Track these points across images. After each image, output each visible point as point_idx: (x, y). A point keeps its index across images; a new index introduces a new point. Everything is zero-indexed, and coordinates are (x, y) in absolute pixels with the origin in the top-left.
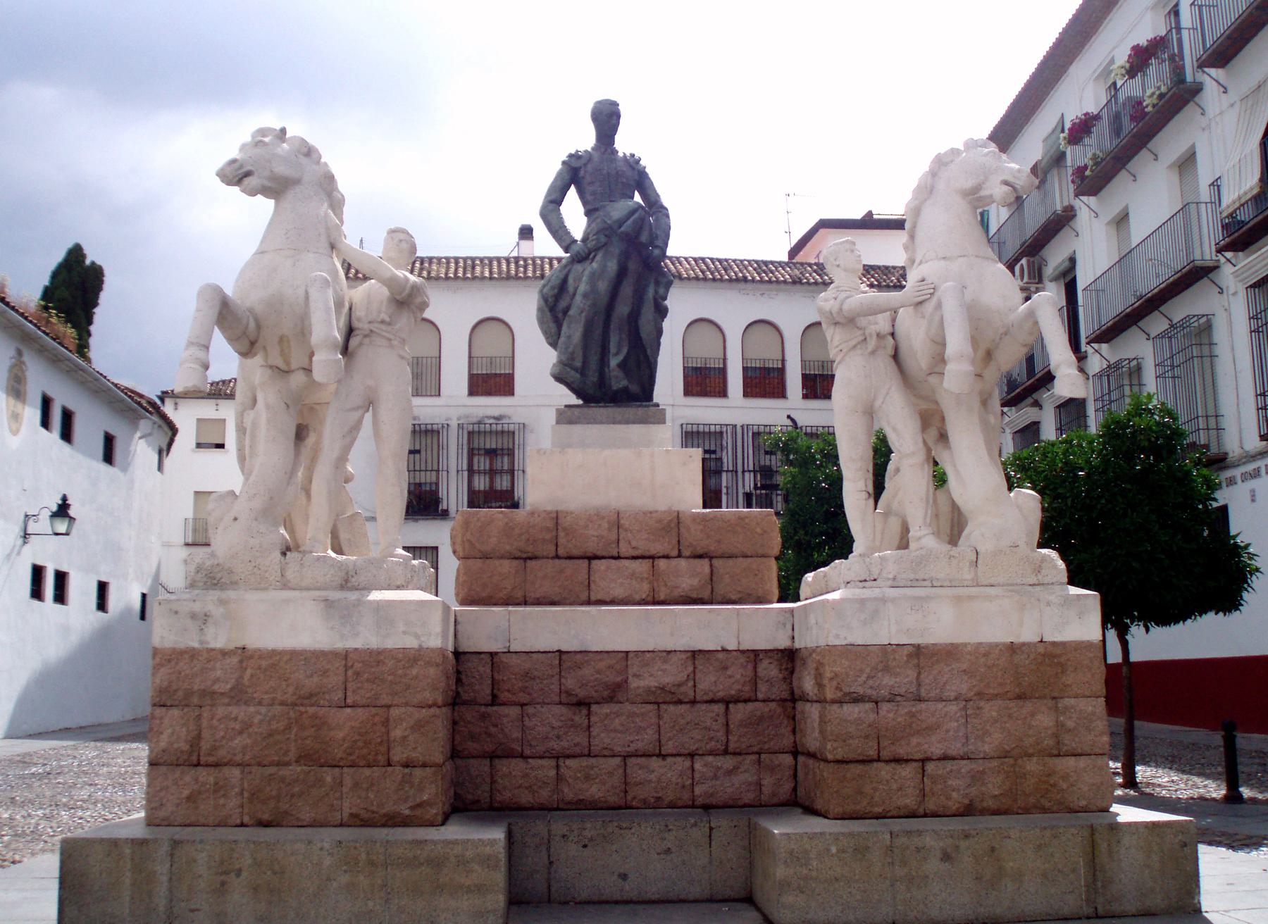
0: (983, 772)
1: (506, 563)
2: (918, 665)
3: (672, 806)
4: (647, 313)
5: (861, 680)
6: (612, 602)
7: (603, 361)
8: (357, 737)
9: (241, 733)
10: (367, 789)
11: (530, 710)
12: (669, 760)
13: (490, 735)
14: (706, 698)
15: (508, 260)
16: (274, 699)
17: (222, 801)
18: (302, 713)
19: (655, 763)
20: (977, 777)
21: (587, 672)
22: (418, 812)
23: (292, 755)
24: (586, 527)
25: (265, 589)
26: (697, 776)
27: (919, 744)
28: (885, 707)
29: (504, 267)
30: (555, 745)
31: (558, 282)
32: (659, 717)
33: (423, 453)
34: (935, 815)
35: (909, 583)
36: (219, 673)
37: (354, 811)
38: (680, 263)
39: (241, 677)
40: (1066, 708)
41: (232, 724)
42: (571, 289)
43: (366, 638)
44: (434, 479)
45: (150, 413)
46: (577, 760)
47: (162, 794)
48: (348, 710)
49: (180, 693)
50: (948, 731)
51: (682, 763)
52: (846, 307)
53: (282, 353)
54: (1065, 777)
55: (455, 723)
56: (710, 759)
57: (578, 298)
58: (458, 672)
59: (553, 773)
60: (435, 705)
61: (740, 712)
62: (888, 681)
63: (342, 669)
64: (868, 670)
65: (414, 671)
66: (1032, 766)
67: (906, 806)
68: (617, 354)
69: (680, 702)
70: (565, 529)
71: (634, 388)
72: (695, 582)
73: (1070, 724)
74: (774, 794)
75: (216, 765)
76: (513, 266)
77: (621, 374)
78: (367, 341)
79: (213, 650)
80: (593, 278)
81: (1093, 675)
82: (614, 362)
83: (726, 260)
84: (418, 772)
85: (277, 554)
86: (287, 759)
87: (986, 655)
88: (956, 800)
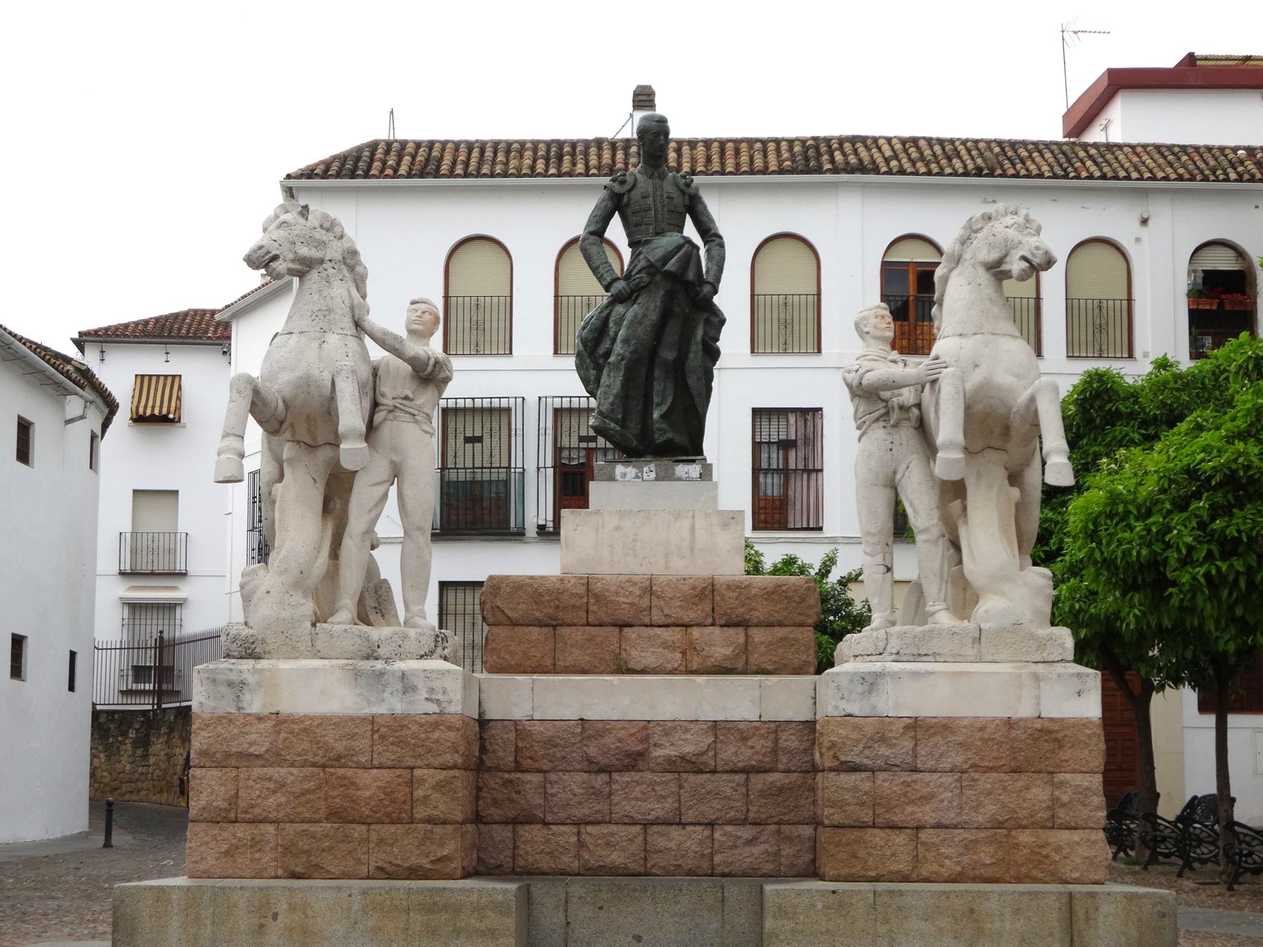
0: (976, 841)
1: (536, 630)
2: (915, 737)
3: (690, 873)
4: (695, 356)
5: (857, 750)
6: (643, 672)
7: (647, 412)
8: (383, 796)
9: (275, 792)
10: (391, 845)
11: (553, 777)
12: (689, 828)
13: (512, 801)
14: (726, 768)
15: (613, 145)
16: (306, 760)
17: (258, 856)
18: (332, 774)
19: (675, 832)
20: (969, 846)
21: (609, 740)
22: (439, 866)
23: (322, 814)
24: (617, 594)
25: (297, 658)
26: (716, 846)
27: (913, 813)
28: (882, 776)
29: (607, 155)
30: (578, 813)
31: (599, 323)
32: (681, 787)
33: (486, 440)
34: (927, 880)
35: (912, 658)
36: (254, 736)
37: (380, 864)
38: (879, 149)
39: (276, 740)
40: (1062, 782)
41: (268, 785)
42: (611, 333)
43: (391, 704)
44: (503, 476)
45: (82, 388)
46: (598, 827)
47: (203, 849)
48: (374, 771)
49: (218, 755)
50: (942, 801)
51: (700, 832)
52: (864, 382)
53: (309, 430)
54: (1058, 849)
55: (479, 789)
56: (729, 828)
57: (618, 348)
58: (481, 738)
59: (574, 839)
60: (455, 767)
61: (758, 781)
62: (883, 751)
63: (369, 734)
64: (865, 740)
65: (436, 735)
66: (1025, 837)
67: (899, 872)
68: (659, 405)
69: (700, 772)
70: (595, 596)
71: (681, 439)
72: (728, 651)
73: (1065, 798)
74: (792, 866)
75: (252, 822)
76: (620, 155)
77: (664, 426)
78: (391, 415)
79: (249, 715)
80: (636, 322)
81: (1090, 752)
82: (656, 415)
83: (952, 141)
84: (438, 830)
85: (308, 625)
86: (317, 816)
87: (982, 729)
88: (950, 866)
